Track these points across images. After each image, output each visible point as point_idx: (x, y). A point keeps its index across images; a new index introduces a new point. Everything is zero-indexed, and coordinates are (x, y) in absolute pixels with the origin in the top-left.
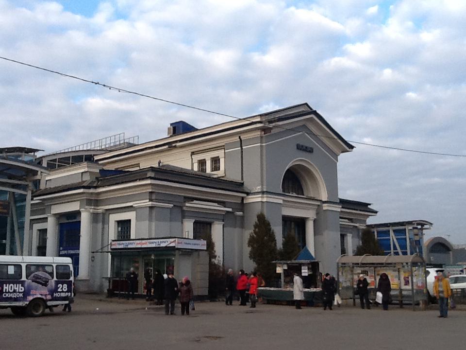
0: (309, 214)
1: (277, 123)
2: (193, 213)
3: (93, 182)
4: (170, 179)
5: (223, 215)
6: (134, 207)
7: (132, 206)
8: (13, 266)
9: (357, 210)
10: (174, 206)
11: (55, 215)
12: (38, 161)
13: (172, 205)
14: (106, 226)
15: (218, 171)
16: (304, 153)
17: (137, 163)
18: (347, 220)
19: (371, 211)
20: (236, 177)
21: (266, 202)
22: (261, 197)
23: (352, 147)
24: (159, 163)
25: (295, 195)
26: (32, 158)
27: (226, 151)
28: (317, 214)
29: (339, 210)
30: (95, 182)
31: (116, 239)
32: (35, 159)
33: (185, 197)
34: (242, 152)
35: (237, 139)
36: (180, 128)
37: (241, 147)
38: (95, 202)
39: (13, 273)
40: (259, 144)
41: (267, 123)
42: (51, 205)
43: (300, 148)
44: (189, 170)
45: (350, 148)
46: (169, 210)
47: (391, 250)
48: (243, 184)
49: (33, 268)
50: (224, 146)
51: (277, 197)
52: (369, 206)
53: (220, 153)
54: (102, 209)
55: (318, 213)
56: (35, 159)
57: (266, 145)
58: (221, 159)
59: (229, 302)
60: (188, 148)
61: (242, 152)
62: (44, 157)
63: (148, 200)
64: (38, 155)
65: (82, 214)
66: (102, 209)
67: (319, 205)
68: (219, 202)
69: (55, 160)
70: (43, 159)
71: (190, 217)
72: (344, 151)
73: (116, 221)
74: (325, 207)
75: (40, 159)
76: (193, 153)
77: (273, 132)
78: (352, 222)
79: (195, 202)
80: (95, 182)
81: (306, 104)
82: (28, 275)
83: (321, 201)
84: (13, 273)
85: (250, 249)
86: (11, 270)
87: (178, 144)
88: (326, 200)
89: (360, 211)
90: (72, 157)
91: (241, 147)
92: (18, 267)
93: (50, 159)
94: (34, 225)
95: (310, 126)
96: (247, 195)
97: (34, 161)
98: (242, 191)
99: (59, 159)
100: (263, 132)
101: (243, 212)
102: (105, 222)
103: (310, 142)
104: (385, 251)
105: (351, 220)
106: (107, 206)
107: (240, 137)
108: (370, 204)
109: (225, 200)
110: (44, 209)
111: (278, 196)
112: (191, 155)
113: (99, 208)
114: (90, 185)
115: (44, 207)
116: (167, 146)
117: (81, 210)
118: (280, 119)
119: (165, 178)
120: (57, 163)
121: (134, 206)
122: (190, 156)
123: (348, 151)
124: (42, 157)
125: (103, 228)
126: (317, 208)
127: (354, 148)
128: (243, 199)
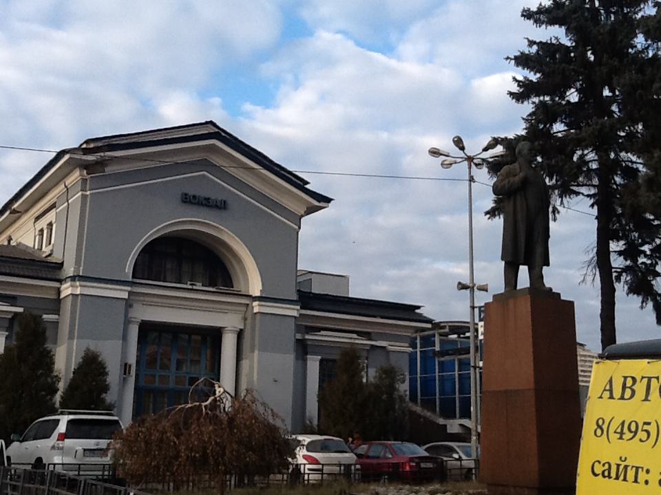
0: (229, 322)
5: (368, 350)
16: (195, 208)
18: (355, 336)
19: (422, 319)
20: (57, 258)
21: (259, 312)
22: (72, 286)
23: (328, 200)
25: (199, 286)
29: (295, 314)
33: (306, 327)
43: (189, 200)
44: (27, 247)
45: (319, 202)
48: (62, 263)
51: (95, 284)
52: (417, 311)
57: (91, 194)
63: (407, 345)
67: (248, 305)
68: (358, 333)
72: (312, 210)
77: (109, 170)
78: (370, 339)
79: (323, 333)
81: (211, 123)
82: (315, 462)
83: (250, 296)
88: (258, 294)
95: (218, 160)
100: (85, 172)
101: (59, 315)
103: (218, 187)
105: (368, 335)
108: (419, 307)
109: (14, 293)
123: (325, 207)
127: (332, 202)
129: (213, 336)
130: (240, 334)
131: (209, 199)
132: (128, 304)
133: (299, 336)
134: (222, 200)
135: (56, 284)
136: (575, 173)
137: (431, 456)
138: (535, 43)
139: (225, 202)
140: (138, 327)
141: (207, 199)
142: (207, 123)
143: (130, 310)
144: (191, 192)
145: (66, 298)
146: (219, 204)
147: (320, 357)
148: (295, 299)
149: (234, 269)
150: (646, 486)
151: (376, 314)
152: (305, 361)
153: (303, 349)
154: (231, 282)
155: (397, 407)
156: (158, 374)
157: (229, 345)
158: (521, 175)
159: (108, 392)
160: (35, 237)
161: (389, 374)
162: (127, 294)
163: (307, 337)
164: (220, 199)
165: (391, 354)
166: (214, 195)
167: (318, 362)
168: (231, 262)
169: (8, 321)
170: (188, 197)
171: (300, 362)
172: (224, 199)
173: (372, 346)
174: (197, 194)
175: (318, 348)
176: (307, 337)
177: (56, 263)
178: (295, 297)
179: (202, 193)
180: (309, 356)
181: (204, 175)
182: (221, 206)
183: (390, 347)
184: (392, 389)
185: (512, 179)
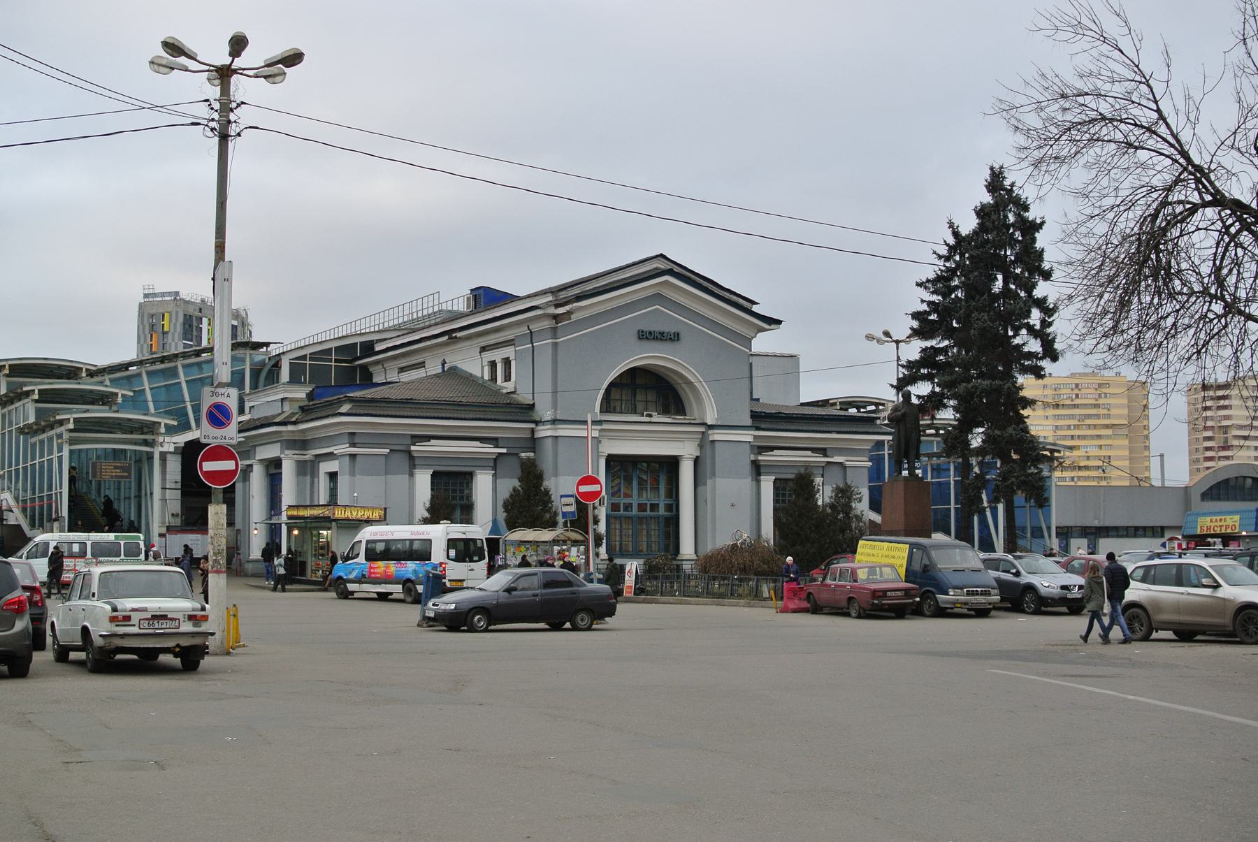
0: (686, 450)
1: (575, 305)
2: (427, 460)
3: (293, 414)
4: (374, 413)
6: (336, 454)
7: (332, 453)
8: (78, 544)
9: (830, 432)
10: (390, 450)
11: (261, 461)
12: (273, 362)
13: (388, 451)
14: (316, 480)
15: (509, 383)
17: (422, 360)
18: (809, 453)
20: (524, 397)
24: (444, 363)
26: (264, 357)
27: (517, 349)
28: (701, 446)
30: (297, 413)
31: (326, 503)
32: (269, 358)
33: (413, 437)
34: (533, 351)
35: (524, 330)
36: (485, 297)
37: (533, 346)
38: (302, 444)
39: (78, 550)
40: (550, 341)
41: (553, 308)
42: (255, 446)
43: (644, 336)
44: (475, 376)
45: (770, 325)
46: (384, 458)
47: (950, 505)
48: (534, 405)
49: (1035, 529)
50: (513, 340)
53: (509, 352)
54: (311, 453)
55: (705, 443)
56: (269, 358)
58: (512, 362)
59: (279, 586)
60: (476, 341)
61: (533, 351)
62: (283, 353)
63: (348, 445)
64: (274, 350)
65: (254, 466)
66: (311, 453)
67: (703, 432)
69: (304, 357)
70: (282, 357)
71: (427, 466)
73: (326, 473)
74: (717, 435)
75: (277, 358)
76: (483, 349)
77: (574, 317)
78: (825, 456)
79: (776, 452)
80: (297, 413)
84: (78, 550)
85: (505, 514)
86: (76, 548)
87: (459, 334)
89: (838, 432)
90: (335, 348)
91: (533, 346)
92: (83, 545)
93: (294, 357)
94: (320, 464)
95: (668, 292)
96: (536, 425)
97: (267, 360)
98: (529, 419)
99: (310, 354)
101: (535, 452)
102: (314, 474)
103: (668, 320)
104: (933, 507)
105: (824, 452)
106: (317, 450)
107: (528, 327)
110: (249, 450)
111: (581, 424)
112: (480, 352)
113: (305, 453)
114: (286, 421)
115: (249, 449)
116: (445, 338)
117: (282, 456)
118: (579, 298)
119: (366, 412)
120: (308, 362)
121: (335, 452)
122: (479, 354)
124: (279, 354)
125: (312, 483)
126: (700, 436)
128: (533, 431)
129: (671, 465)
130: (697, 461)
131: (664, 333)
132: (597, 441)
133: (753, 457)
134: (674, 333)
135: (532, 426)
136: (937, 405)
137: (1248, 534)
138: (925, 301)
139: (678, 334)
140: (605, 460)
141: (662, 334)
142: (657, 256)
143: (600, 445)
144: (646, 329)
145: (545, 439)
146: (672, 337)
147: (774, 478)
148: (749, 425)
149: (689, 400)
150: (184, 544)
151: (830, 429)
152: (758, 481)
153: (757, 469)
154: (683, 407)
155: (854, 525)
156: (622, 502)
157: (686, 473)
158: (903, 411)
159: (599, 523)
160: (483, 367)
161: (845, 493)
162: (598, 432)
163: (760, 458)
164: (673, 332)
165: (848, 469)
166: (669, 328)
167: (772, 483)
168: (685, 392)
169: (493, 461)
170: (644, 333)
171: (754, 482)
172: (679, 331)
173: (827, 462)
174: (652, 329)
175: (772, 467)
176: (760, 458)
177: (529, 405)
178: (749, 422)
179: (656, 327)
180: (762, 477)
181: (657, 309)
182: (675, 338)
183: (847, 463)
184: (847, 509)
185: (897, 413)
